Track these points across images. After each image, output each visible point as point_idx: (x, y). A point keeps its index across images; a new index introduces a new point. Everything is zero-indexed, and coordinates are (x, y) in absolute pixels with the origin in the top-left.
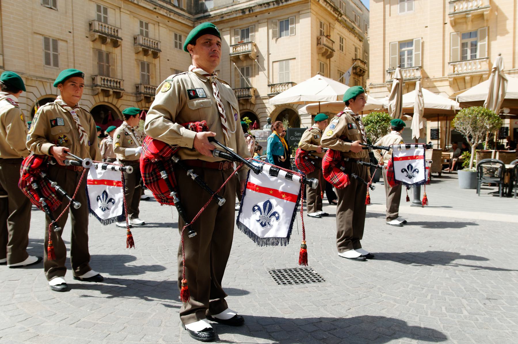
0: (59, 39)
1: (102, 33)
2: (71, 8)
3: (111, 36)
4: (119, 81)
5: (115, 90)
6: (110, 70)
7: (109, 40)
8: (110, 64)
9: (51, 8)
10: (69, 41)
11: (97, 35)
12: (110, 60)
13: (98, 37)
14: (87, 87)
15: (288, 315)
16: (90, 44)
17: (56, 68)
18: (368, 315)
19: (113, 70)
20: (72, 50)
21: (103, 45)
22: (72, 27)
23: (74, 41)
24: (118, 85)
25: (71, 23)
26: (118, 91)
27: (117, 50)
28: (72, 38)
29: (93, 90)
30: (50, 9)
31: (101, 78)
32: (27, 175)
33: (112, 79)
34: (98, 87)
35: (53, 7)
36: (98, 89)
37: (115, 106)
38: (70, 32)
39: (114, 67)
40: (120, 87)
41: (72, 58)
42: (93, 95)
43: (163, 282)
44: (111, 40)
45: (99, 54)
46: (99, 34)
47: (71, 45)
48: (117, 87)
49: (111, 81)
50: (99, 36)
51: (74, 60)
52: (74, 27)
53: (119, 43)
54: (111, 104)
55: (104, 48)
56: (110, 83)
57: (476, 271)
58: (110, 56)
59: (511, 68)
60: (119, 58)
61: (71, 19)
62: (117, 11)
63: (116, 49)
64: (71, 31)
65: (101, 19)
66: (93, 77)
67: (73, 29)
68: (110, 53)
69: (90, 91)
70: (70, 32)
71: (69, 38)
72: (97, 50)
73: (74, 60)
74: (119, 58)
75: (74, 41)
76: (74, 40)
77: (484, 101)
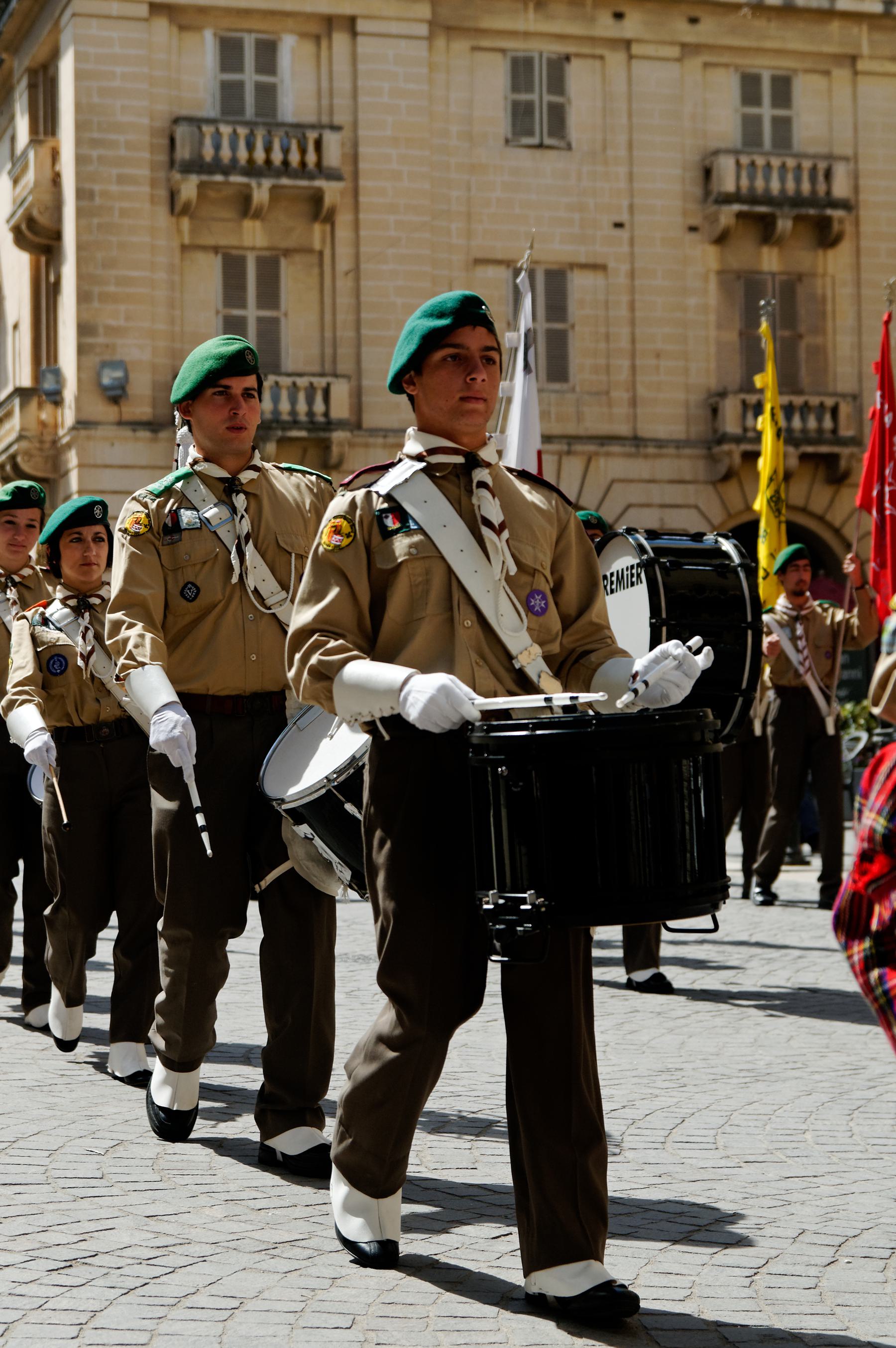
0: (573, 266)
1: (753, 199)
2: (624, 120)
3: (797, 201)
4: (829, 402)
5: (810, 449)
6: (802, 354)
7: (784, 225)
8: (802, 328)
9: (541, 146)
10: (611, 265)
11: (727, 215)
12: (802, 311)
13: (732, 221)
14: (687, 451)
15: (366, 1274)
16: (706, 257)
17: (556, 386)
18: (566, 1334)
19: (819, 353)
20: (625, 299)
21: (765, 250)
22: (625, 203)
23: (632, 263)
24: (828, 424)
25: (623, 185)
26: (824, 449)
27: (836, 262)
28: (626, 249)
29: (712, 459)
30: (538, 153)
31: (744, 403)
32: (876, 868)
33: (814, 401)
34: (726, 447)
35: (547, 141)
36: (729, 454)
37: (821, 519)
38: (619, 225)
39: (819, 340)
40: (834, 431)
41: (625, 331)
42: (714, 483)
43: (713, 1322)
44: (797, 219)
45: (746, 290)
46: (736, 207)
47: (622, 280)
48: (820, 430)
49: (805, 409)
50: (740, 215)
51: (633, 341)
52: (637, 201)
53: (836, 227)
54: (804, 510)
55: (770, 260)
56: (804, 419)
57: (443, 1106)
58: (801, 291)
59: (565, 460)
60: (845, 293)
61: (622, 170)
62: (841, 74)
63: (831, 253)
64: (624, 217)
65: (759, 134)
66: (713, 400)
67: (631, 208)
68: (800, 277)
69: (701, 465)
70: (619, 225)
71: (609, 248)
72: (739, 275)
73: (633, 341)
74: (845, 293)
75: (632, 263)
76: (632, 255)
77: (599, 555)
